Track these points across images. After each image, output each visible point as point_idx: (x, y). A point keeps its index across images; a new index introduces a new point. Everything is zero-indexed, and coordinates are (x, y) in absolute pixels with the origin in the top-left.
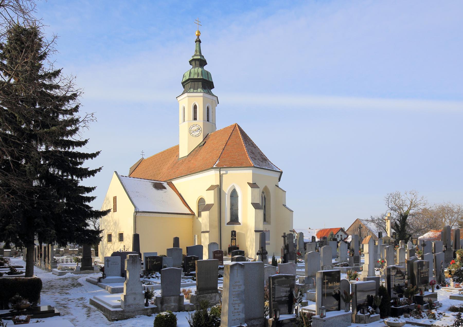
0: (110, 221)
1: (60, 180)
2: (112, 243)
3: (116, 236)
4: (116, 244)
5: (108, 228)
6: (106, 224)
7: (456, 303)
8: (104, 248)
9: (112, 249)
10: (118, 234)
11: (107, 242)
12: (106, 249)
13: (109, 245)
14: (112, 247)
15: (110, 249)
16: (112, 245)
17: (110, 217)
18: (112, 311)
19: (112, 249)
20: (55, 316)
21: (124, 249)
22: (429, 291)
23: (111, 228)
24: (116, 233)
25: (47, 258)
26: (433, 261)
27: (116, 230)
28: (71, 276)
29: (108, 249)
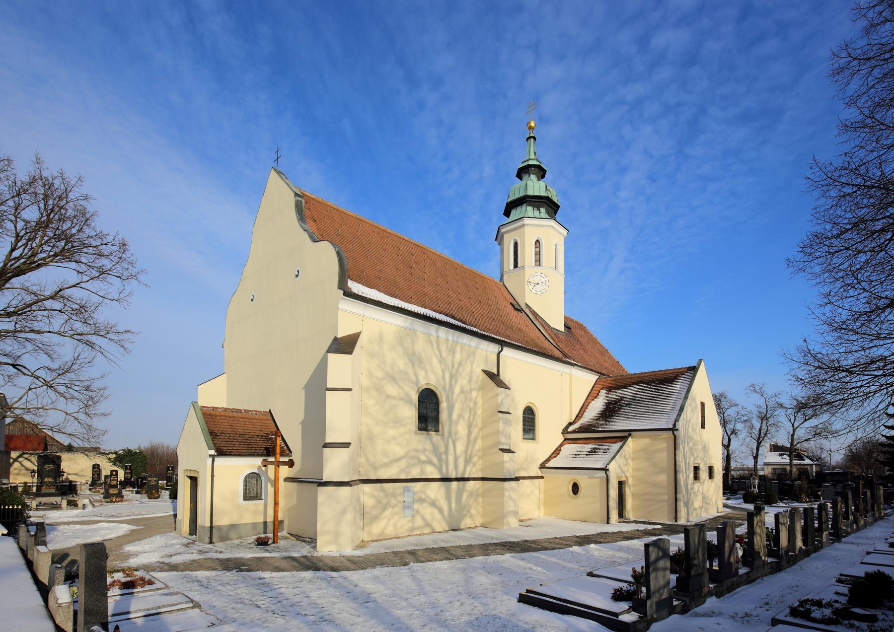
0: (698, 441)
1: (816, 525)
2: (700, 482)
3: (706, 470)
4: (706, 482)
5: (695, 454)
6: (691, 444)
7: (61, 315)
8: (690, 491)
9: (700, 493)
10: (708, 467)
11: (693, 479)
12: (692, 495)
13: (697, 485)
14: (701, 489)
15: (698, 494)
16: (701, 485)
17: (698, 435)
18: (652, 623)
19: (700, 493)
20: (623, 602)
21: (126, 301)
22: (746, 513)
23: (700, 455)
24: (705, 464)
25: (231, 453)
26: (608, 518)
27: (705, 459)
28: (32, 552)
29: (694, 493)
